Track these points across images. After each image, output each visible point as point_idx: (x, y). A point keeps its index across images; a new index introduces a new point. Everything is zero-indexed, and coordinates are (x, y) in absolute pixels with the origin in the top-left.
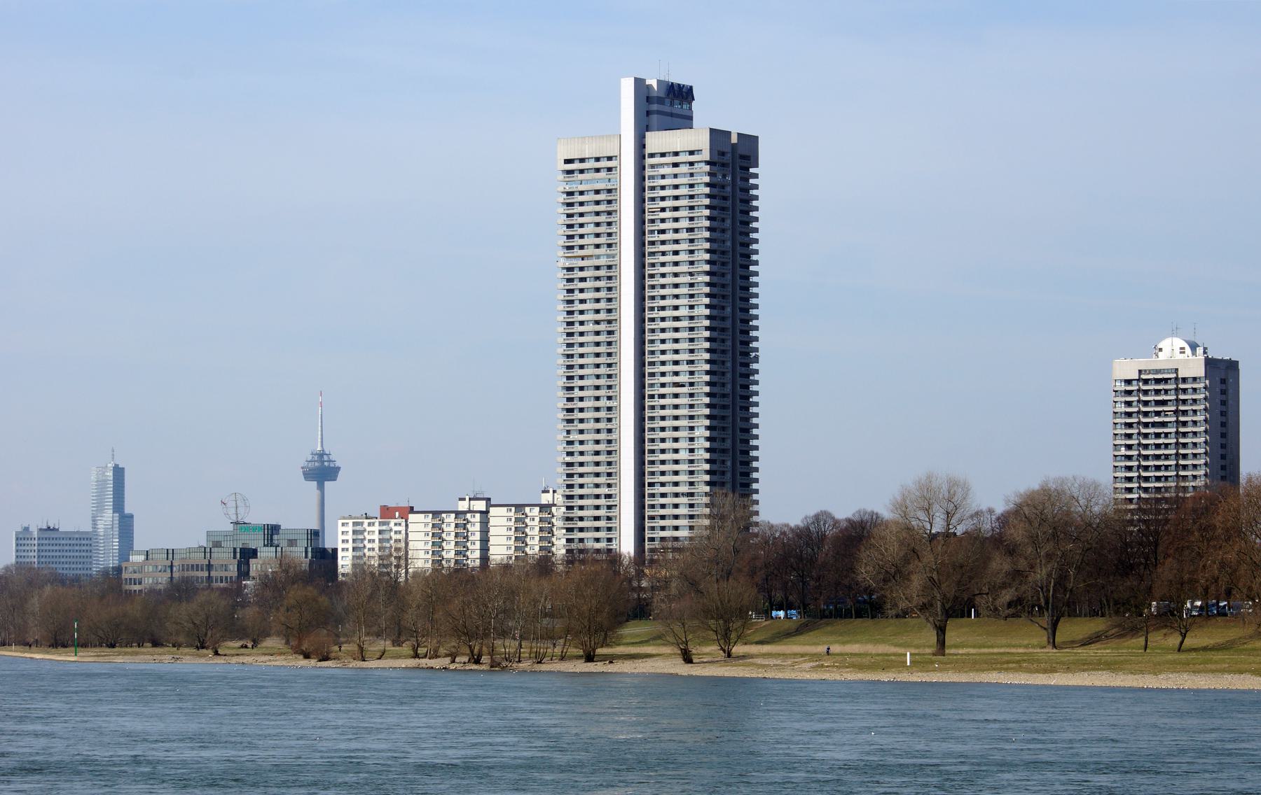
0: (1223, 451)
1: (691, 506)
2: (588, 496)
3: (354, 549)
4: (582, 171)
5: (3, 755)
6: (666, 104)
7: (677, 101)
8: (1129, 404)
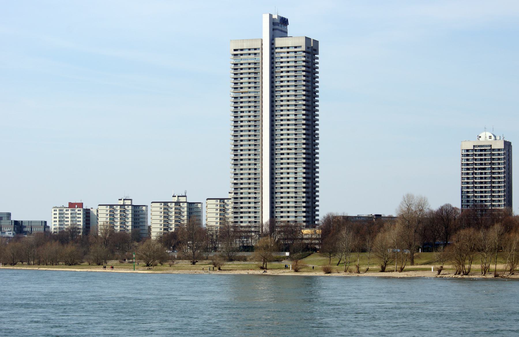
1: (296, 202)
2: (245, 198)
3: (59, 221)
4: (242, 55)
5: (517, 320)
6: (279, 26)
8: (468, 160)
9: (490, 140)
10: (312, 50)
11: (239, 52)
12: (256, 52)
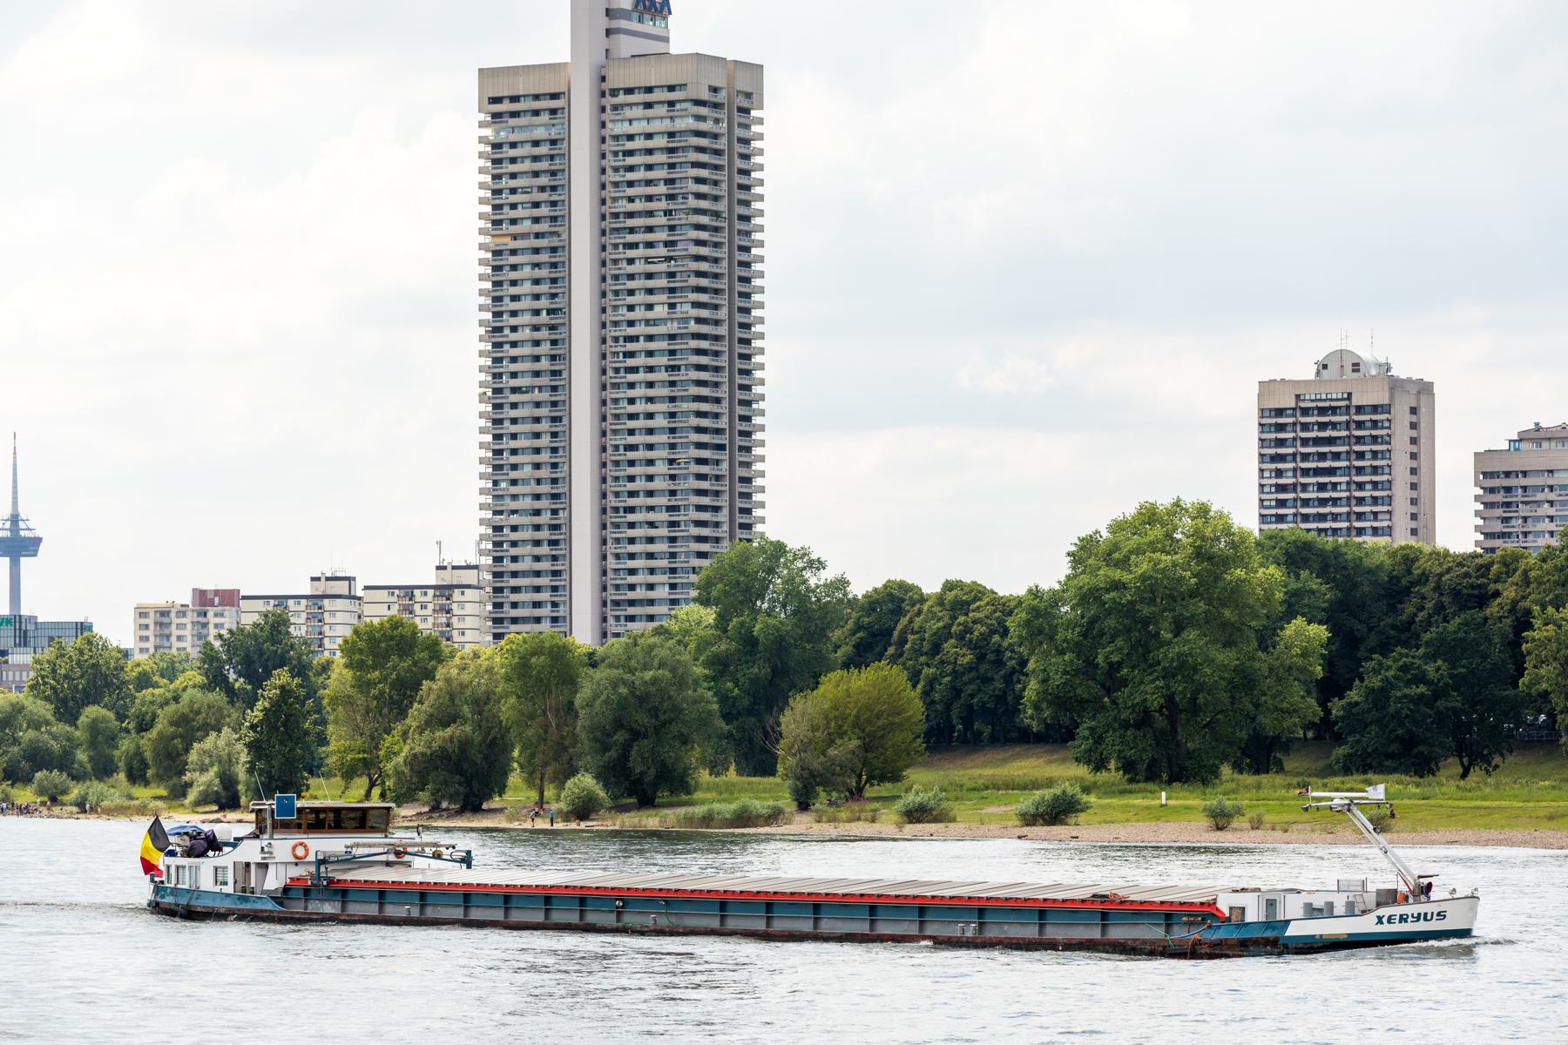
0: (1414, 510)
2: (524, 574)
4: (514, 114)
7: (647, 17)
9: (1356, 375)
10: (1455, 941)
11: (505, 106)
12: (553, 103)
